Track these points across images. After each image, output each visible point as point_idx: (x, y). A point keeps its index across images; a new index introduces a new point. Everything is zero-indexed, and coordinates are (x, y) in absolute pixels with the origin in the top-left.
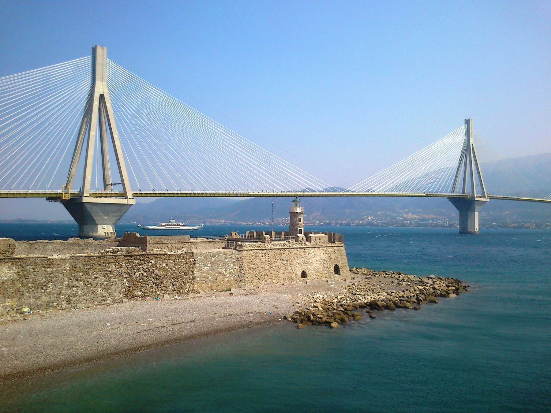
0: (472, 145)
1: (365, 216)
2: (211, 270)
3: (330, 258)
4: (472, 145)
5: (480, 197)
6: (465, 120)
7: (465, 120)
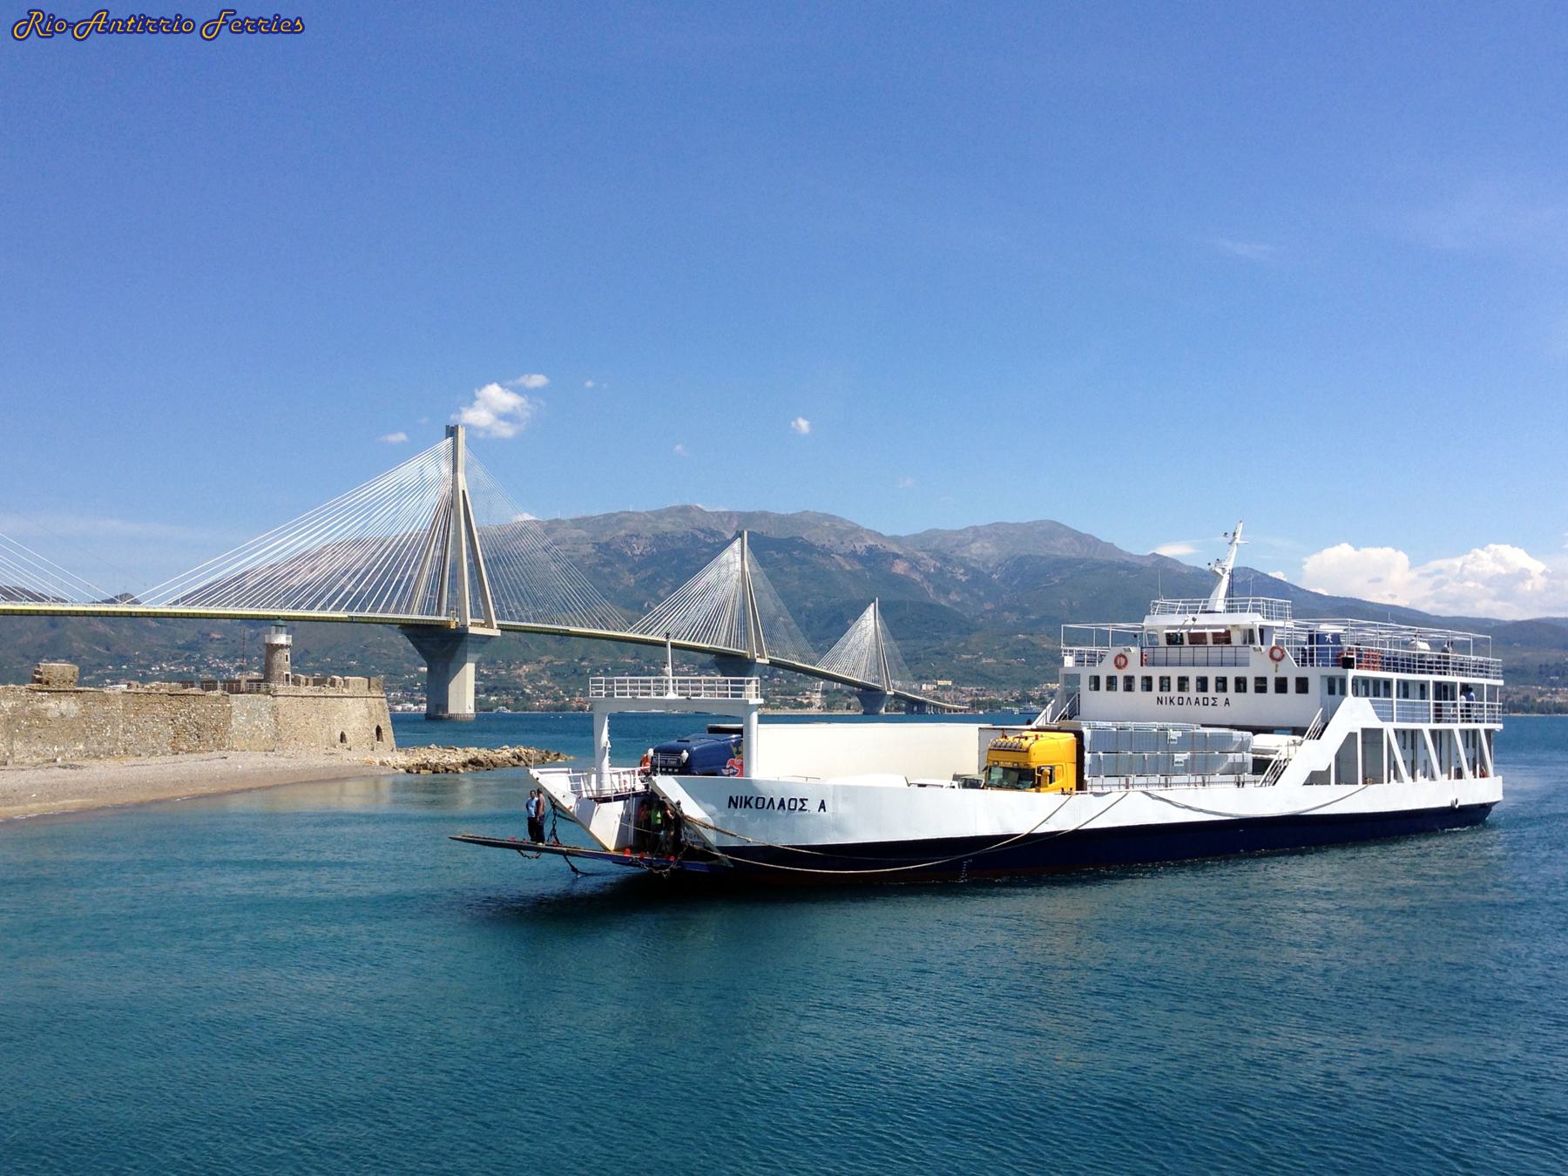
1: (108, 681)
2: (248, 722)
3: (371, 715)
6: (447, 427)
7: (447, 427)
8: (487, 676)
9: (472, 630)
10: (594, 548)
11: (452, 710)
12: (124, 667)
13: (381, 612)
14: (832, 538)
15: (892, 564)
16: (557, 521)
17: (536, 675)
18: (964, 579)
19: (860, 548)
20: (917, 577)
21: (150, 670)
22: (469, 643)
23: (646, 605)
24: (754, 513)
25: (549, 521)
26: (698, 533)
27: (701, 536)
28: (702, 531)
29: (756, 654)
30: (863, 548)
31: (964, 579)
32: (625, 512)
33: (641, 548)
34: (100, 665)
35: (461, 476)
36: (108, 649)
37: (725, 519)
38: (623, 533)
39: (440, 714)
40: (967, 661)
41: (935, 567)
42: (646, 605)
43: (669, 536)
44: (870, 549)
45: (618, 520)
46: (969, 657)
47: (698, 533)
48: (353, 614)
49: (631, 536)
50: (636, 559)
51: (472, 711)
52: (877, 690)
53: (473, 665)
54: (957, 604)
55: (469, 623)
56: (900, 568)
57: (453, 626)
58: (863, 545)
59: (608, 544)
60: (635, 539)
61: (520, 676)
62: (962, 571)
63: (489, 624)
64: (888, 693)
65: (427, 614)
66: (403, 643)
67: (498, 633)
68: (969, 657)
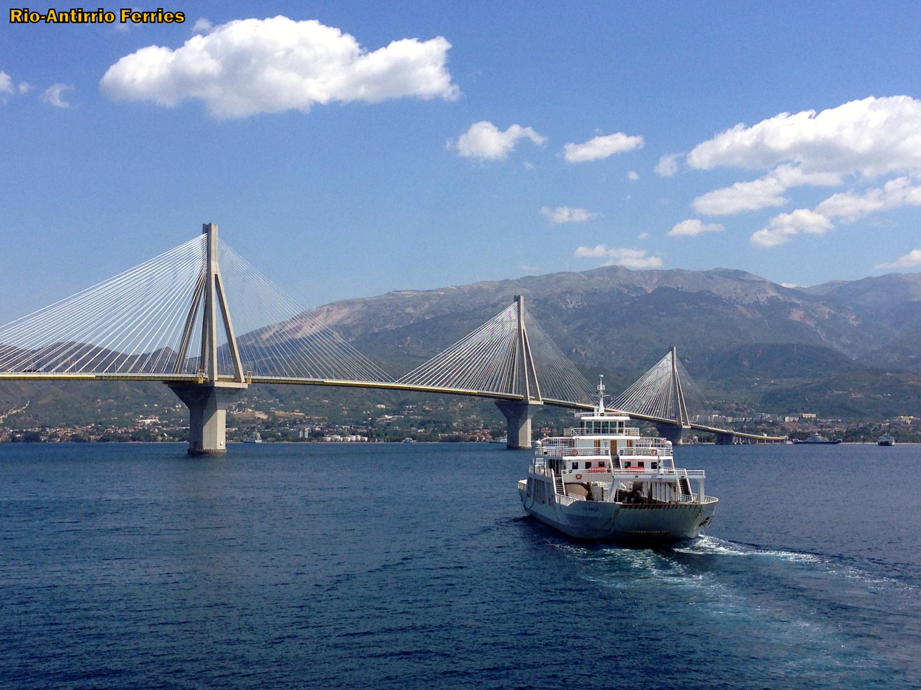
0: (216, 276)
1: (141, 416)
4: (216, 276)
5: (233, 380)
6: (204, 225)
7: (204, 225)
8: (429, 411)
9: (217, 384)
10: (534, 303)
11: (205, 447)
12: (156, 405)
13: (166, 372)
14: (739, 291)
15: (789, 313)
16: (507, 281)
17: (468, 410)
18: (855, 324)
19: (762, 299)
20: (811, 323)
21: (175, 408)
22: (217, 395)
23: (574, 350)
24: (671, 271)
25: (500, 282)
26: (622, 289)
27: (625, 291)
28: (625, 286)
29: (529, 397)
30: (765, 298)
31: (855, 324)
32: (563, 273)
33: (574, 303)
34: (137, 404)
35: (214, 264)
36: (144, 391)
37: (647, 277)
38: (559, 290)
39: (197, 450)
40: (838, 396)
41: (829, 313)
42: (574, 350)
43: (598, 291)
44: (771, 300)
45: (557, 279)
46: (840, 392)
47: (622, 289)
48: (103, 374)
49: (566, 293)
50: (570, 312)
51: (223, 447)
52: (672, 424)
53: (224, 411)
54: (845, 346)
55: (216, 378)
56: (796, 315)
57: (201, 381)
58: (765, 296)
59: (546, 300)
60: (568, 295)
61: (455, 412)
62: (854, 317)
63: (237, 379)
64: (684, 427)
65: (180, 373)
66: (168, 393)
67: (246, 386)
68: (840, 392)
